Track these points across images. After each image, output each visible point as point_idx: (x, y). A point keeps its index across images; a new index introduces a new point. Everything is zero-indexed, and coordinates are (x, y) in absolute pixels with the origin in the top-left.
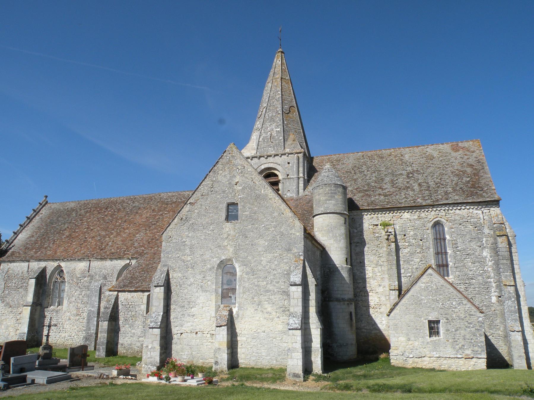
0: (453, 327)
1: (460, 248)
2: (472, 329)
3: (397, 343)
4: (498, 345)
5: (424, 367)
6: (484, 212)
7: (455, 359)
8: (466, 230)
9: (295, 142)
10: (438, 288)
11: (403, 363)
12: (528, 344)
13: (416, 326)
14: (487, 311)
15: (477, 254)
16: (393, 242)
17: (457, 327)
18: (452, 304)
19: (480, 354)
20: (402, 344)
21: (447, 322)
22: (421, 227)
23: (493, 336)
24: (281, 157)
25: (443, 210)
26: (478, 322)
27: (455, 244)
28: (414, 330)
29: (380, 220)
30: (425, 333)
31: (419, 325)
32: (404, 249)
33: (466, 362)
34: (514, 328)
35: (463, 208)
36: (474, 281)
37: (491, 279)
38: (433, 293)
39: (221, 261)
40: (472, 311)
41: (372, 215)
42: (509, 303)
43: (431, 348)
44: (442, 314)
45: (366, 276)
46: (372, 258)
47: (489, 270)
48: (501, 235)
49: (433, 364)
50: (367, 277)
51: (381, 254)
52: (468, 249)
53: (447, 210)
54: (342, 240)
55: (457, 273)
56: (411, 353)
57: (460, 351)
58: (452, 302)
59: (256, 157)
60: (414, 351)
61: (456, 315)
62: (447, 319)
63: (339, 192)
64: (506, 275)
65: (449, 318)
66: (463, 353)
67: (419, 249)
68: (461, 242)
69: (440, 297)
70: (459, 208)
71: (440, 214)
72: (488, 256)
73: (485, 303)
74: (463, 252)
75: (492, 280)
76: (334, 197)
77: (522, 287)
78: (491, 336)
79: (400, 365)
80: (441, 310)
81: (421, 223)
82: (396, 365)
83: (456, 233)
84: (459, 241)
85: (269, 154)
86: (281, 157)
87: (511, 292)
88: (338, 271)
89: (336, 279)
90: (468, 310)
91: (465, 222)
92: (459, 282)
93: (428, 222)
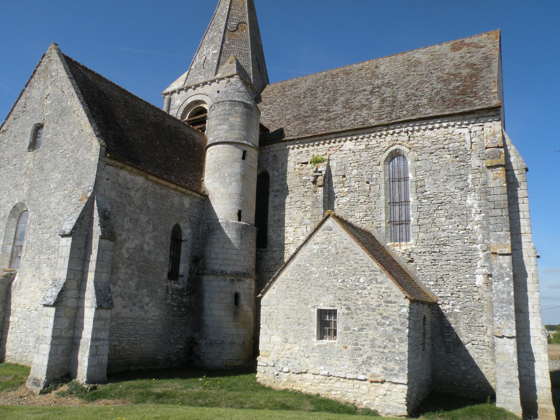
0: (356, 324)
1: (428, 193)
2: (387, 329)
3: (269, 345)
4: (480, 361)
5: (304, 391)
6: (473, 130)
7: (355, 381)
8: (440, 163)
9: (232, 65)
10: (338, 253)
11: (273, 380)
12: (535, 361)
13: (299, 319)
14: (467, 300)
15: (456, 201)
16: (320, 186)
17: (362, 323)
18: (358, 281)
19: (395, 375)
20: (275, 347)
21: (348, 314)
22: (368, 161)
23: (473, 344)
24: (210, 85)
25: (405, 132)
26: (400, 315)
27: (421, 187)
28: (294, 324)
29: (312, 155)
30: (312, 332)
31: (303, 317)
32: (341, 198)
33: (372, 389)
34: (502, 331)
35: (437, 125)
36: (449, 247)
37: (477, 244)
38: (329, 262)
39: (15, 207)
40: (392, 295)
41: (301, 149)
42: (500, 286)
43: (317, 359)
44: (340, 300)
45: (284, 240)
46: (295, 213)
47: (475, 229)
48: (494, 164)
49: (319, 387)
50: (286, 242)
51: (308, 207)
52: (442, 195)
53: (411, 131)
54: (234, 184)
55: (421, 235)
56: (287, 364)
57: (363, 366)
58: (359, 277)
59: (182, 89)
60: (292, 360)
61: (364, 300)
62: (348, 309)
63: (237, 112)
64: (499, 236)
65: (351, 307)
66: (368, 371)
67: (364, 197)
68: (430, 184)
69: (340, 268)
70: (430, 126)
71: (400, 138)
72: (475, 206)
73: (463, 287)
74: (432, 199)
75: (479, 246)
76: (228, 119)
77: (533, 259)
78: (470, 344)
79: (268, 384)
80: (339, 292)
81: (369, 155)
82: (262, 383)
83: (424, 168)
84: (428, 181)
85: (197, 83)
86: (210, 85)
87: (505, 265)
88: (221, 228)
89: (215, 240)
90: (384, 293)
91: (440, 149)
92: (423, 250)
93: (380, 152)
